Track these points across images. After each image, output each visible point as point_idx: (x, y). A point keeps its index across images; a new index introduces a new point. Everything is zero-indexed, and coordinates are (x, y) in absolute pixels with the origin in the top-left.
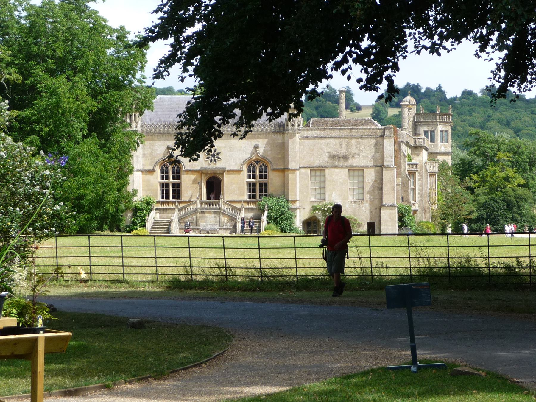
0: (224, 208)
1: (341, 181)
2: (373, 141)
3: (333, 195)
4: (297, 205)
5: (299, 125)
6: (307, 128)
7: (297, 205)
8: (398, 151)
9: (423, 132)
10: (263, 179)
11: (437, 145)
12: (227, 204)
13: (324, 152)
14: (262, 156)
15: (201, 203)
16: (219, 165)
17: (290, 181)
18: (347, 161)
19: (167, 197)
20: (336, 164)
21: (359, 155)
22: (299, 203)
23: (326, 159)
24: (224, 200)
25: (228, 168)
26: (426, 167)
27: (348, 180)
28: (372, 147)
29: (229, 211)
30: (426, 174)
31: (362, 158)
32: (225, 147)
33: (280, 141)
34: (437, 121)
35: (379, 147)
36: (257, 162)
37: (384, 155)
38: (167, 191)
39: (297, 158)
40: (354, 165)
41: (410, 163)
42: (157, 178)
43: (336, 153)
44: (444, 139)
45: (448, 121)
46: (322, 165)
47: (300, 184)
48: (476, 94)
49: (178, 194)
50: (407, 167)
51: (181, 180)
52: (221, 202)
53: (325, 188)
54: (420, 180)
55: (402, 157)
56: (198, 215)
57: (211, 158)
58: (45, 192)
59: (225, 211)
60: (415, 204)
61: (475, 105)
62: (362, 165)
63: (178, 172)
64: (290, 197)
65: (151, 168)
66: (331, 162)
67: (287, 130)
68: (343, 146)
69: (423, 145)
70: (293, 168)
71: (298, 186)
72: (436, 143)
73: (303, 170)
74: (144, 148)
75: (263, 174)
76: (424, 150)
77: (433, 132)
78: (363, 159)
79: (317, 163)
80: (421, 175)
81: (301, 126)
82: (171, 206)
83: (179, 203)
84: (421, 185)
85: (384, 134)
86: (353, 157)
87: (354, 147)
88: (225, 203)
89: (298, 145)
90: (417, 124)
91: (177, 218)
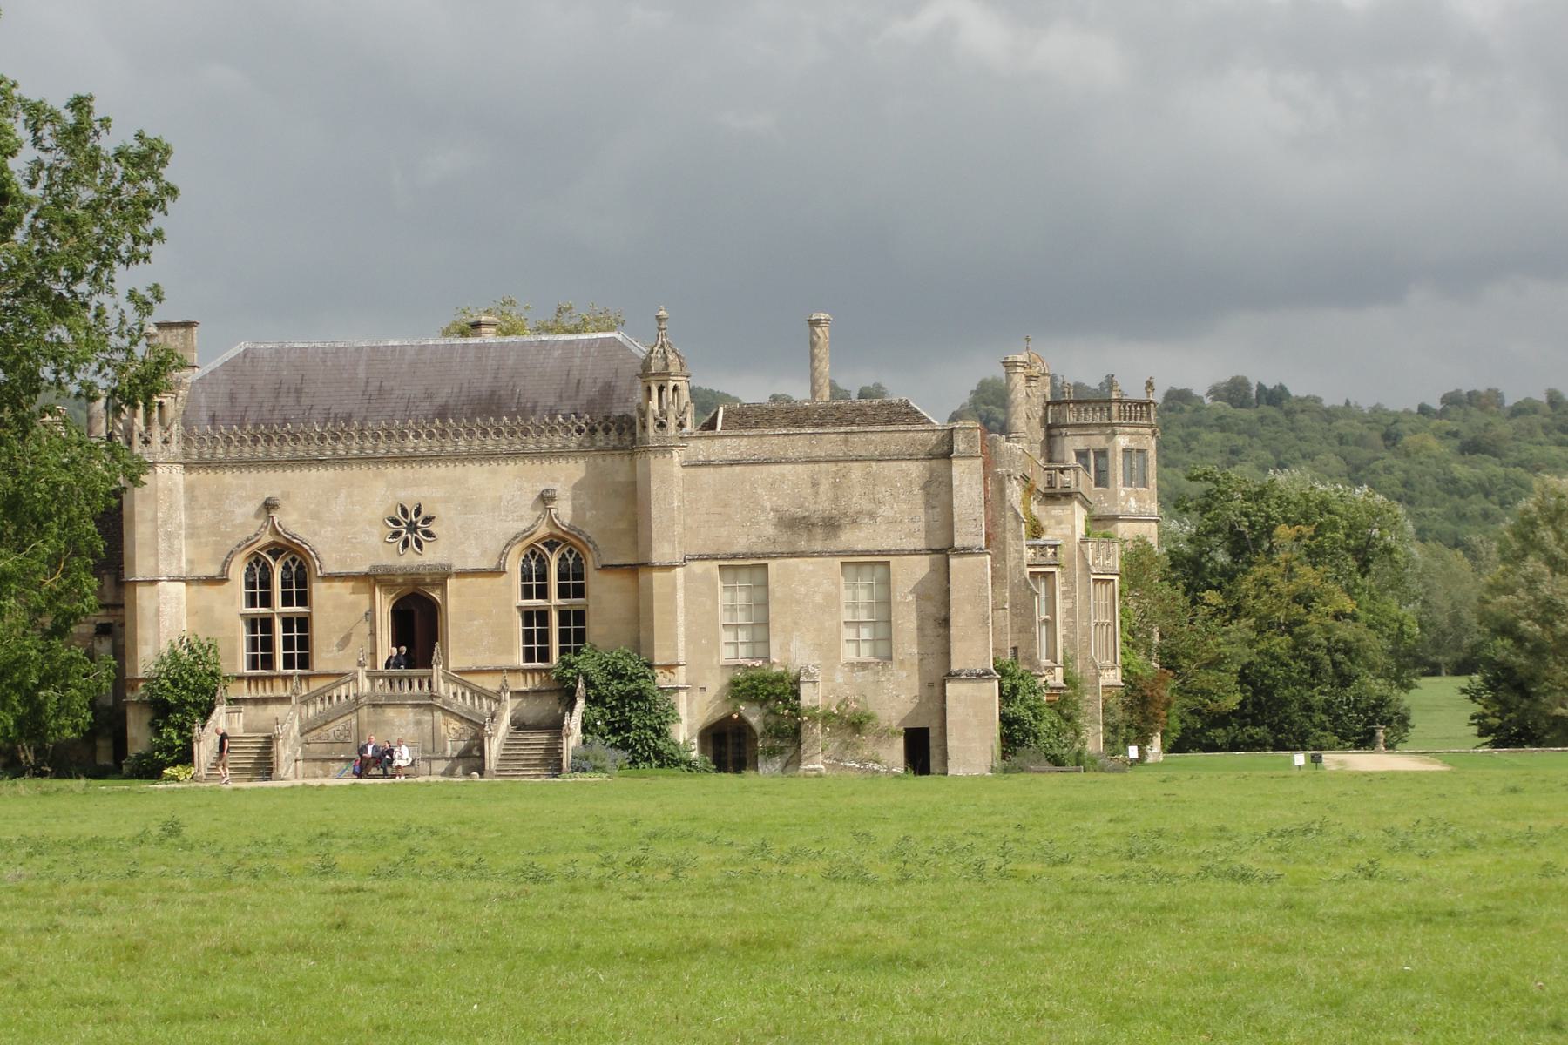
0: (447, 691)
1: (819, 598)
2: (916, 470)
3: (795, 645)
4: (680, 676)
5: (681, 425)
6: (707, 433)
7: (680, 676)
8: (995, 500)
9: (1073, 453)
10: (571, 600)
11: (1115, 493)
12: (454, 681)
13: (763, 509)
14: (570, 527)
15: (373, 677)
16: (431, 556)
17: (656, 605)
18: (836, 536)
19: (268, 662)
20: (803, 545)
21: (872, 516)
22: (687, 672)
23: (770, 531)
24: (446, 666)
25: (458, 565)
26: (1084, 557)
27: (842, 580)
28: (916, 490)
29: (464, 703)
30: (1085, 580)
31: (884, 527)
32: (447, 500)
33: (622, 477)
34: (1114, 421)
35: (938, 493)
36: (551, 543)
37: (952, 514)
38: (268, 644)
39: (678, 529)
40: (859, 547)
41: (1038, 541)
42: (232, 603)
43: (800, 513)
44: (1135, 477)
45: (1146, 422)
46: (757, 549)
47: (687, 613)
48: (1200, 399)
49: (301, 653)
50: (1028, 554)
51: (311, 608)
52: (437, 671)
53: (767, 624)
54: (1066, 595)
55: (1011, 524)
56: (364, 712)
57: (404, 535)
58: (46, 698)
59: (450, 704)
60: (1053, 668)
61: (1198, 423)
62: (885, 547)
63: (303, 582)
64: (657, 653)
65: (213, 570)
66: (784, 541)
67: (644, 441)
68: (822, 489)
69: (1073, 488)
70: (666, 562)
71: (681, 619)
72: (1111, 488)
73: (697, 567)
74: (193, 509)
75: (571, 582)
76: (1076, 504)
77: (1101, 454)
78: (887, 530)
79: (740, 546)
80: (1070, 582)
81: (688, 428)
82: (280, 690)
83: (307, 678)
84: (1071, 613)
85: (951, 450)
86: (854, 522)
87: (858, 490)
88: (447, 678)
89: (678, 489)
90: (1055, 432)
91: (296, 727)
